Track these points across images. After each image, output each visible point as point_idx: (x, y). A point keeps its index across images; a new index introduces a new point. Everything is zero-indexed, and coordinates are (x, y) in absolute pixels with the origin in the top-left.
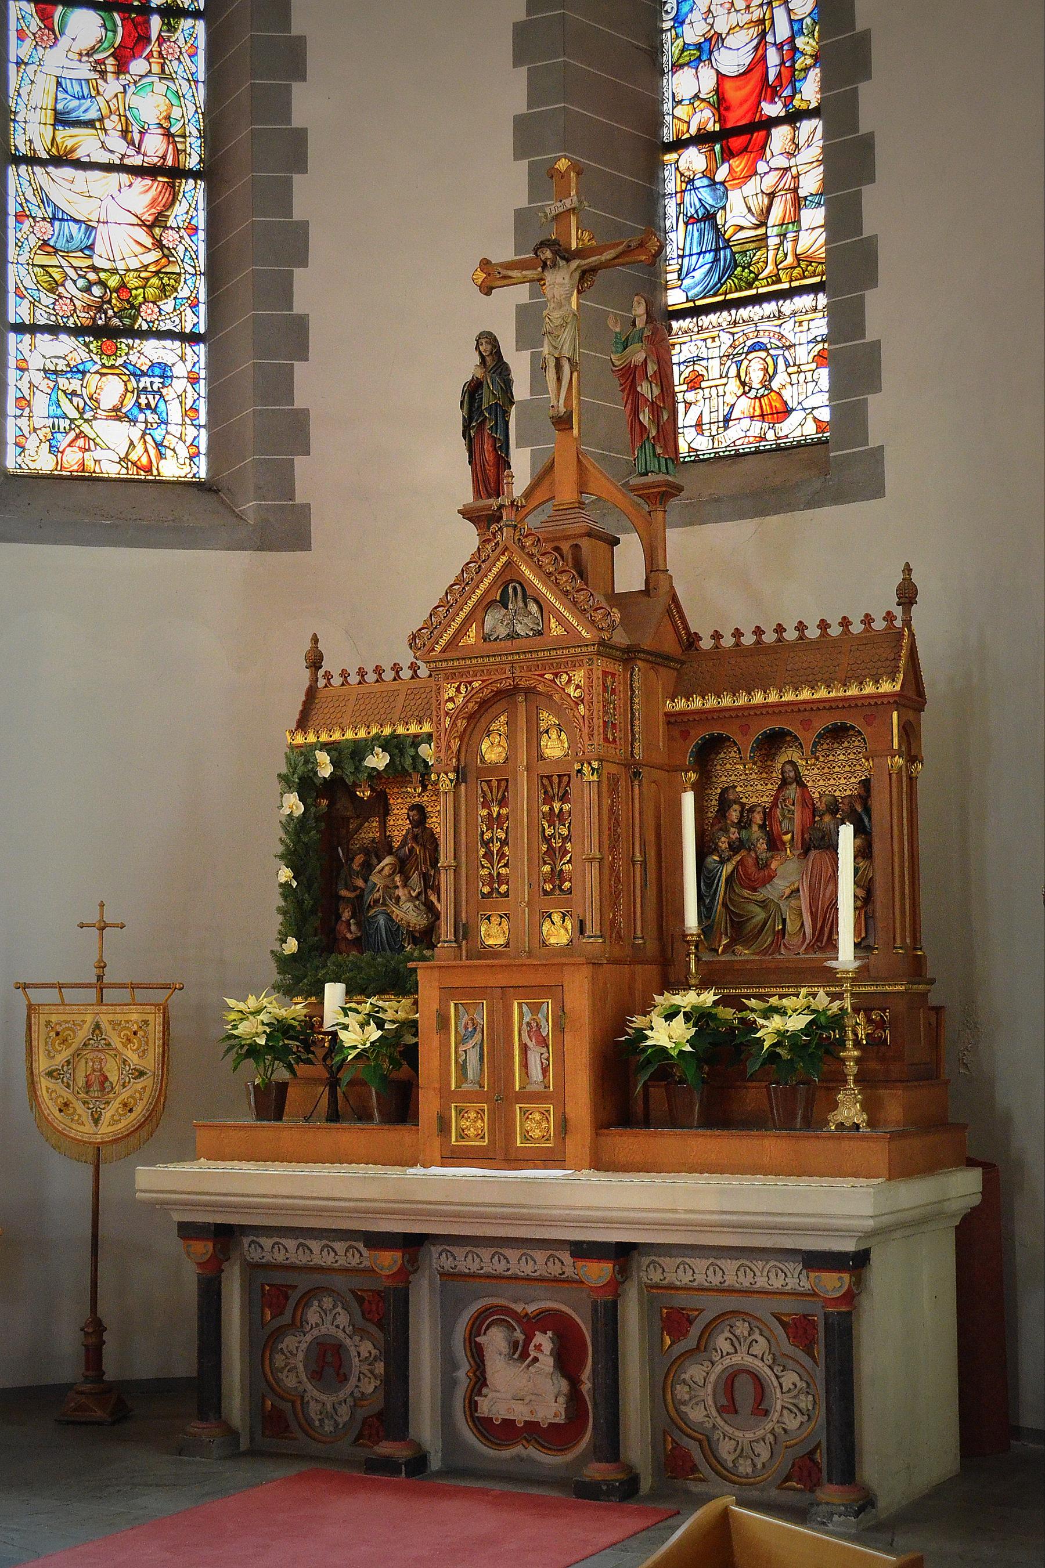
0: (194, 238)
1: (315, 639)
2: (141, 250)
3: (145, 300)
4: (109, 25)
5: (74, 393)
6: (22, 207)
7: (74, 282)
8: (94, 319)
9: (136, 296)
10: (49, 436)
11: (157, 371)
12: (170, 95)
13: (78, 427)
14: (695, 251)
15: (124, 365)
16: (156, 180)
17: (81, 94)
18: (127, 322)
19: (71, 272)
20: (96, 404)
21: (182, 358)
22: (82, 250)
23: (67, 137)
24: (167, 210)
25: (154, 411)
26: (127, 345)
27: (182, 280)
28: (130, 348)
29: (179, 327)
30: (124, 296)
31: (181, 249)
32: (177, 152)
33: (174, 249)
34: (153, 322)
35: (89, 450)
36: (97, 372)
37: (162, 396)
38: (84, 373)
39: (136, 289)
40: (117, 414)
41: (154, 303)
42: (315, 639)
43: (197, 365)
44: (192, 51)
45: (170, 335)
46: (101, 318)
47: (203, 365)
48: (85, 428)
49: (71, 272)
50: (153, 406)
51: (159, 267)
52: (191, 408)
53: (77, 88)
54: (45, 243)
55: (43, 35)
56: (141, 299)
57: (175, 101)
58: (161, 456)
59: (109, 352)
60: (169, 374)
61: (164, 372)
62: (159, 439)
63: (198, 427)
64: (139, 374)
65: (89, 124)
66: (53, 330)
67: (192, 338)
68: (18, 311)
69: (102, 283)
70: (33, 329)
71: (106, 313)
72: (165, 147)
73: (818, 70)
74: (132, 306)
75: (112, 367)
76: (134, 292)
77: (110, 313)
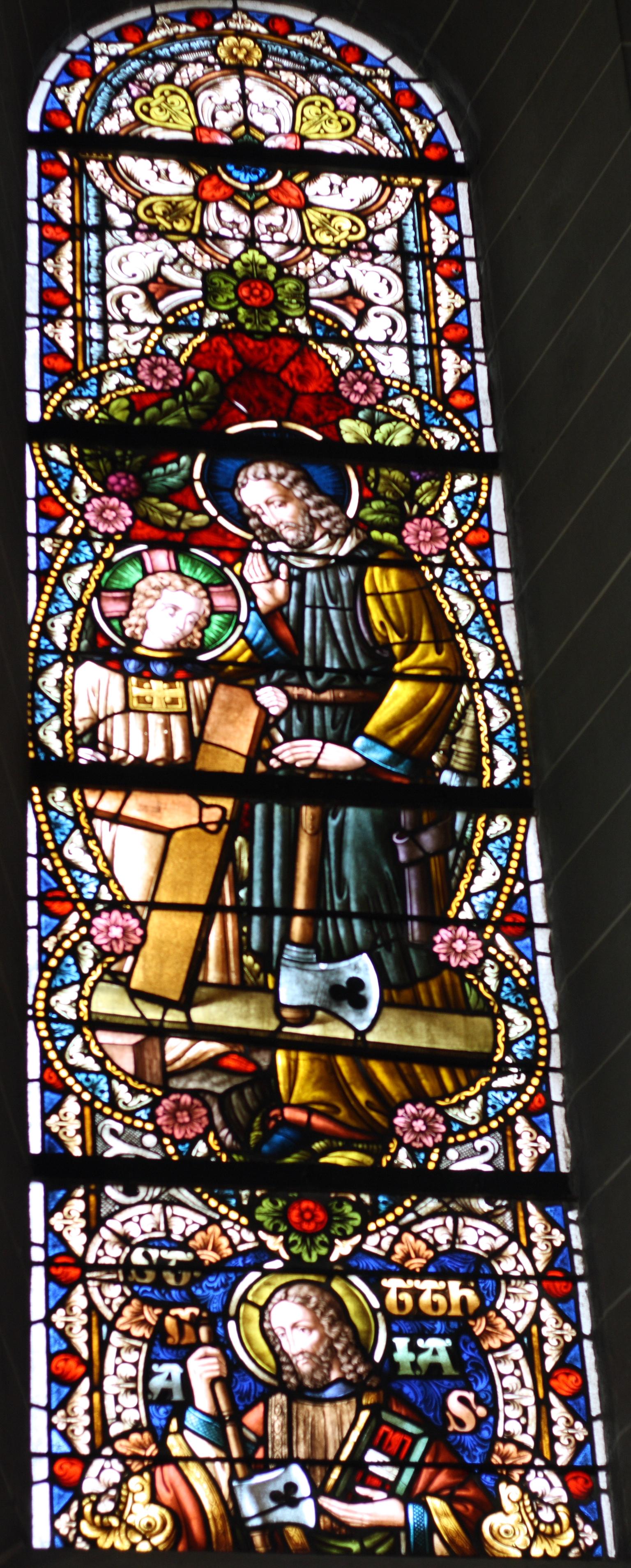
1: (506, 1514)
34: (428, 1151)
42: (506, 1514)
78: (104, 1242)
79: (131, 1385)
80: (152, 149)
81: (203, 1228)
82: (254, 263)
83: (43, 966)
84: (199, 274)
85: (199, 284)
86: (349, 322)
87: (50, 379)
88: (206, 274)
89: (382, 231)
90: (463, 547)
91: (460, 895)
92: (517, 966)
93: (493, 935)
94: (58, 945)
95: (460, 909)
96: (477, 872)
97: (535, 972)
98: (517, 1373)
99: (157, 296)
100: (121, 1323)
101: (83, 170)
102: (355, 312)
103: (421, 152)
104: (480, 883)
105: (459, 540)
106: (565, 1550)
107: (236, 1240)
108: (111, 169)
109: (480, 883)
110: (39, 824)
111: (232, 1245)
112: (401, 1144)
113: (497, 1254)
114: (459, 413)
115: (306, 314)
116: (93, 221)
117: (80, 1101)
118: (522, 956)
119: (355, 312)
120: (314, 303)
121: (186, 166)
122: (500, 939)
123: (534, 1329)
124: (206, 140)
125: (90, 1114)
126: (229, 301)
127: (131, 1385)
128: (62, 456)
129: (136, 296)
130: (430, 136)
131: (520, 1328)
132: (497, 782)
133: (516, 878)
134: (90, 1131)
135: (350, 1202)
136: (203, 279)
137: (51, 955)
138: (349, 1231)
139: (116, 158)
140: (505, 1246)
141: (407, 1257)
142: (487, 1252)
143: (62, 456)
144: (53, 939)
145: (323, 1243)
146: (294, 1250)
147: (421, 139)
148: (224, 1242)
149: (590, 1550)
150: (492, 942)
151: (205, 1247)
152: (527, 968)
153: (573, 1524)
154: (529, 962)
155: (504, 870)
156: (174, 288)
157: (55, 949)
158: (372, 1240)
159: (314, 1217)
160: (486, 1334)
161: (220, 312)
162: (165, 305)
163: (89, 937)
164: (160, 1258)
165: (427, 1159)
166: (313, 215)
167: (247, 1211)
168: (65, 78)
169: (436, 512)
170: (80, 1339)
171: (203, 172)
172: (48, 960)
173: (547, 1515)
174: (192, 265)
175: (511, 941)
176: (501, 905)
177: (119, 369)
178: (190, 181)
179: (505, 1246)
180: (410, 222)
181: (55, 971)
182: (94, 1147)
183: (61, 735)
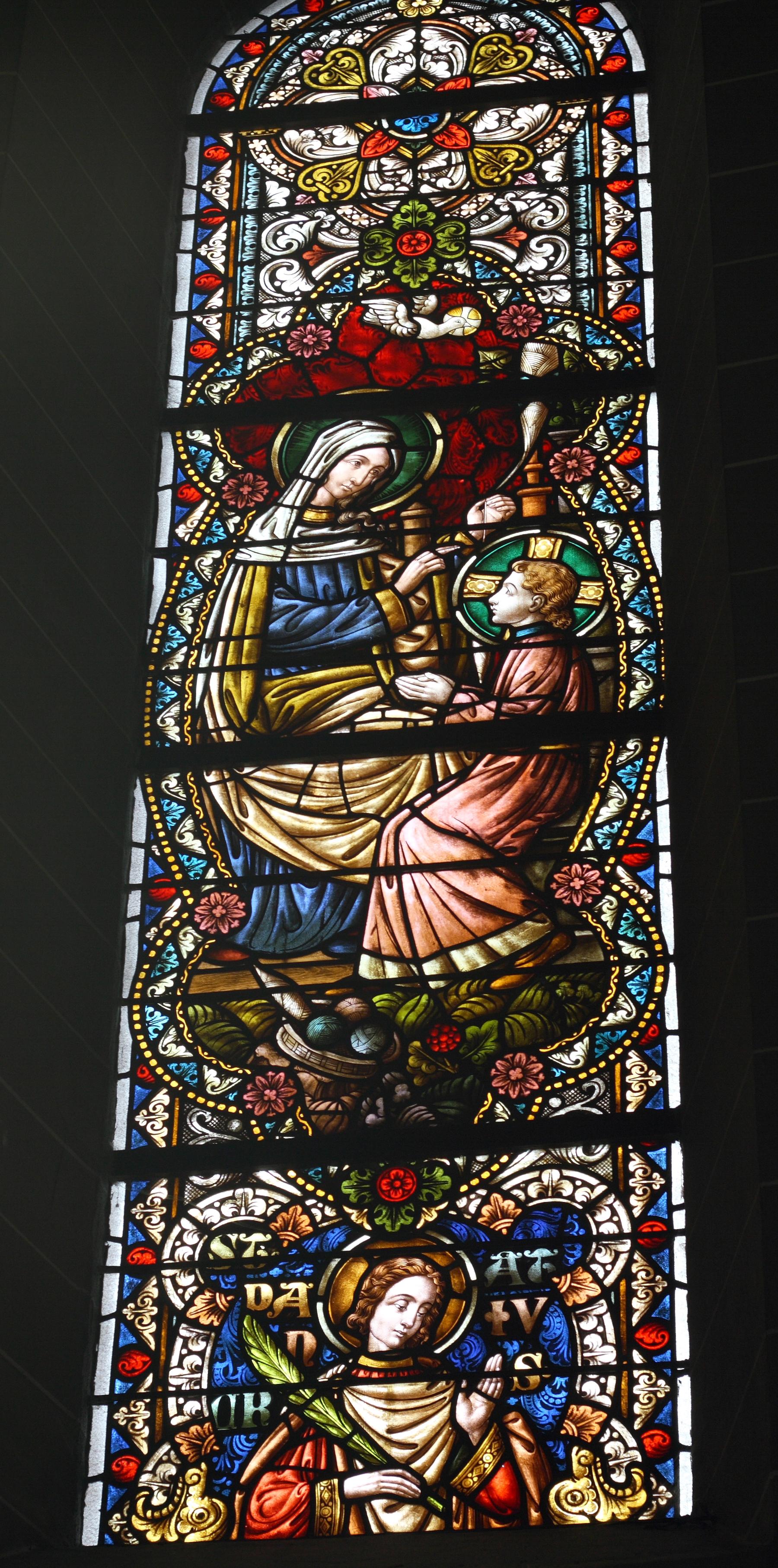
0: (647, 874)
2: (490, 923)
3: (505, 1047)
4: (409, 439)
5: (291, 1318)
6: (166, 866)
7: (301, 1026)
8: (354, 1114)
9: (479, 1040)
10: (210, 1444)
11: (540, 1228)
12: (570, 557)
13: (298, 1409)
14: (230, 661)
15: (443, 1223)
16: (536, 751)
17: (332, 591)
18: (450, 1108)
19: (291, 1005)
20: (353, 1341)
21: (618, 1186)
22: (324, 947)
23: (293, 692)
24: (566, 818)
25: (531, 1343)
26: (451, 1170)
27: (614, 980)
28: (460, 1176)
29: (605, 1104)
30: (444, 1042)
31: (608, 905)
32: (591, 681)
33: (589, 908)
34: (530, 1102)
35: (331, 1471)
36: (359, 1253)
37: (556, 1297)
38: (320, 1260)
39: (478, 1020)
40: (414, 1360)
41: (531, 1050)
43: (663, 1201)
44: (629, 456)
45: (581, 1130)
46: (373, 1109)
47: (678, 1198)
48: (323, 1411)
49: (291, 1005)
50: (528, 1325)
51: (544, 957)
52: (646, 1319)
53: (321, 581)
54: (225, 942)
55: (241, 484)
56: (490, 1045)
57: (583, 569)
58: (554, 1469)
59: (397, 1196)
60: (578, 1230)
61: (565, 1231)
62: (544, 1415)
63: (669, 1371)
64: (483, 1242)
65: (356, 653)
66: (237, 1162)
67: (649, 1128)
68: (139, 1118)
69: (372, 1019)
70: (178, 1162)
71: (388, 1092)
72: (557, 671)
73: (563, 154)
74: (466, 1066)
75: (408, 1232)
76: (471, 1030)
77: (401, 1091)
78: (183, 1231)
79: (505, 120)
80: (320, 117)
81: (285, 1208)
82: (414, 213)
83: (143, 957)
84: (355, 235)
85: (356, 244)
86: (510, 255)
87: (194, 366)
88: (363, 231)
89: (550, 157)
90: (613, 469)
91: (585, 825)
92: (638, 897)
93: (613, 867)
94: (159, 935)
95: (583, 843)
96: (603, 802)
97: (656, 901)
98: (600, 1329)
99: (311, 263)
100: (191, 1313)
101: (246, 149)
102: (517, 244)
103: (598, 65)
104: (606, 813)
105: (610, 462)
106: (636, 1512)
107: (319, 1218)
108: (274, 143)
109: (606, 813)
110: (150, 814)
111: (313, 1222)
112: (497, 1098)
113: (592, 1206)
114: (621, 327)
115: (466, 255)
116: (251, 204)
117: (172, 1093)
118: (643, 885)
119: (517, 244)
120: (475, 242)
121: (351, 126)
122: (620, 870)
123: (623, 1283)
124: (374, 96)
125: (181, 1109)
126: (387, 256)
127: (505, 120)
128: (205, 439)
129: (290, 268)
130: (609, 46)
131: (608, 1282)
132: (632, 704)
133: (645, 804)
134: (177, 1120)
135: (442, 1165)
136: (360, 240)
137: (152, 945)
138: (437, 1197)
139: (281, 134)
140: (193, 1220)
141: (494, 1218)
142: (582, 1203)
143: (205, 439)
144: (154, 930)
145: (408, 1213)
146: (377, 1221)
147: (599, 51)
148: (305, 1219)
149: (662, 1510)
150: (613, 878)
151: (285, 1229)
152: (648, 897)
153: (647, 1485)
154: (650, 891)
155: (632, 797)
156: (331, 251)
157: (156, 939)
158: (462, 1203)
159: (391, 1184)
160: (572, 1290)
161: (376, 269)
162: (318, 273)
163: (190, 922)
164: (238, 1240)
165: (528, 1111)
166: (479, 153)
167: (331, 1184)
168: (237, 59)
169: (585, 440)
170: (148, 1331)
171: (368, 128)
172: (148, 951)
173: (619, 1477)
174: (350, 226)
175: (632, 871)
176: (626, 833)
177: (265, 344)
178: (353, 140)
179: (193, 1220)
180: (581, 140)
181: (153, 962)
182: (179, 1139)
183: (180, 722)
